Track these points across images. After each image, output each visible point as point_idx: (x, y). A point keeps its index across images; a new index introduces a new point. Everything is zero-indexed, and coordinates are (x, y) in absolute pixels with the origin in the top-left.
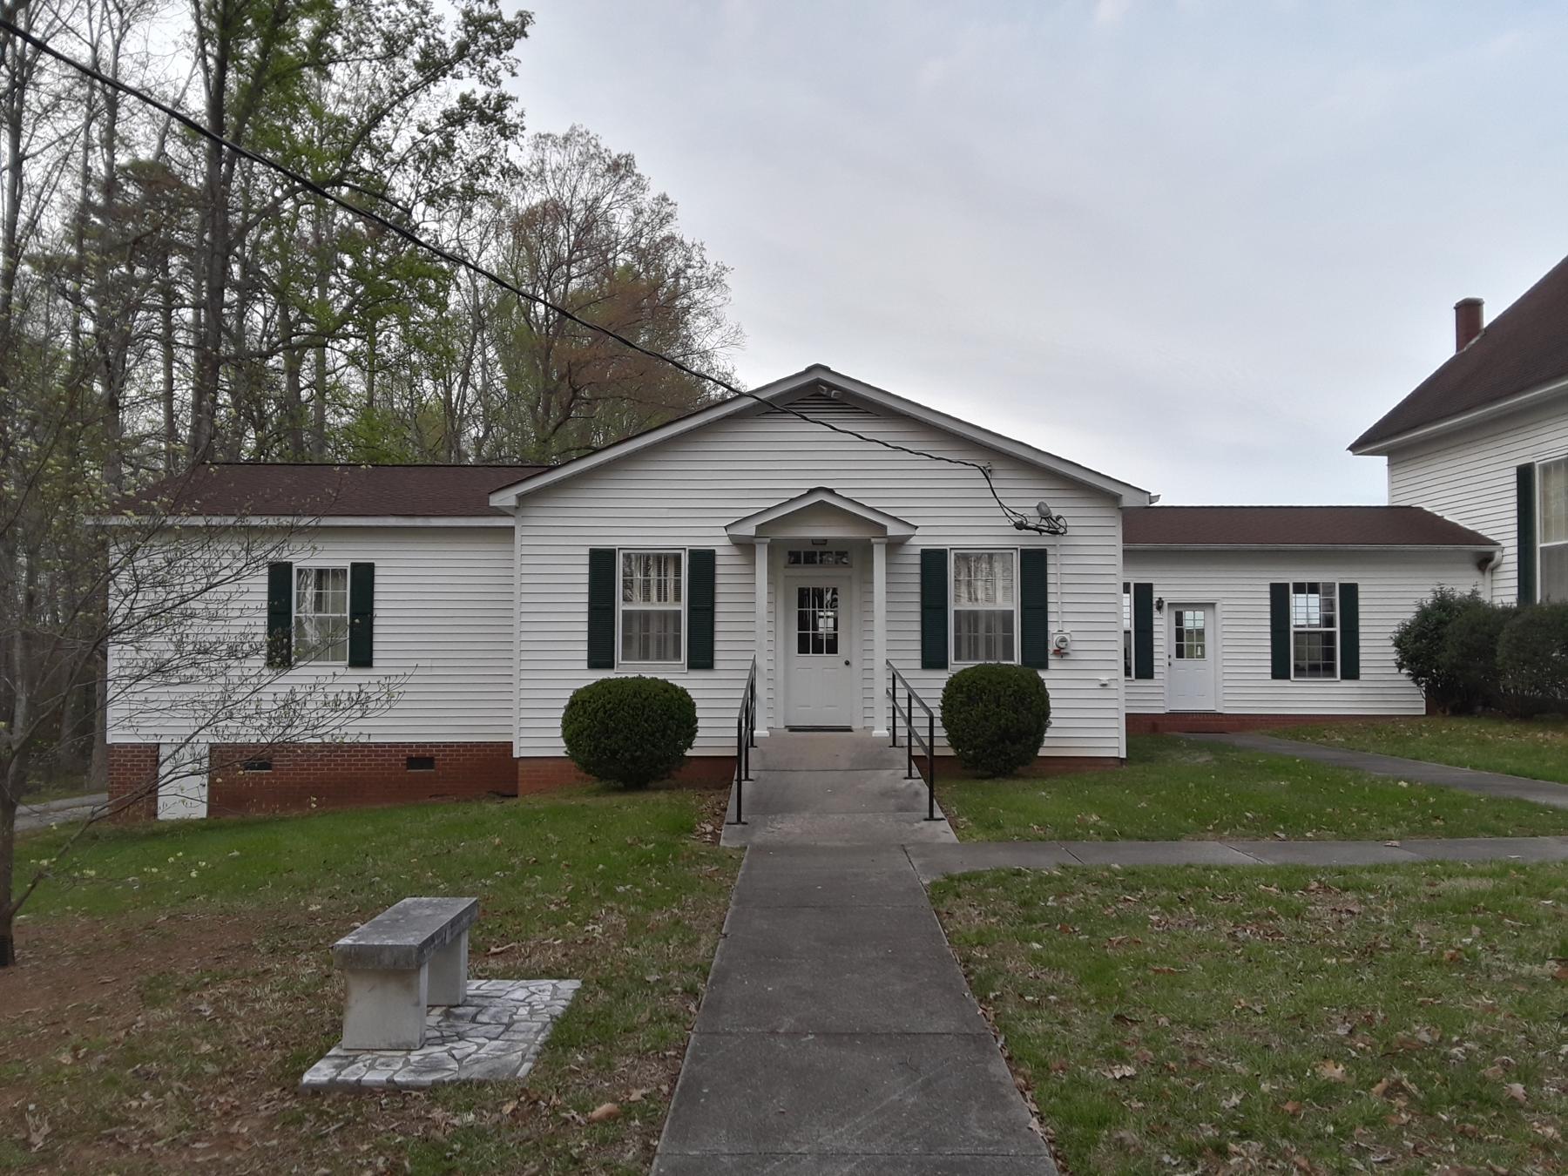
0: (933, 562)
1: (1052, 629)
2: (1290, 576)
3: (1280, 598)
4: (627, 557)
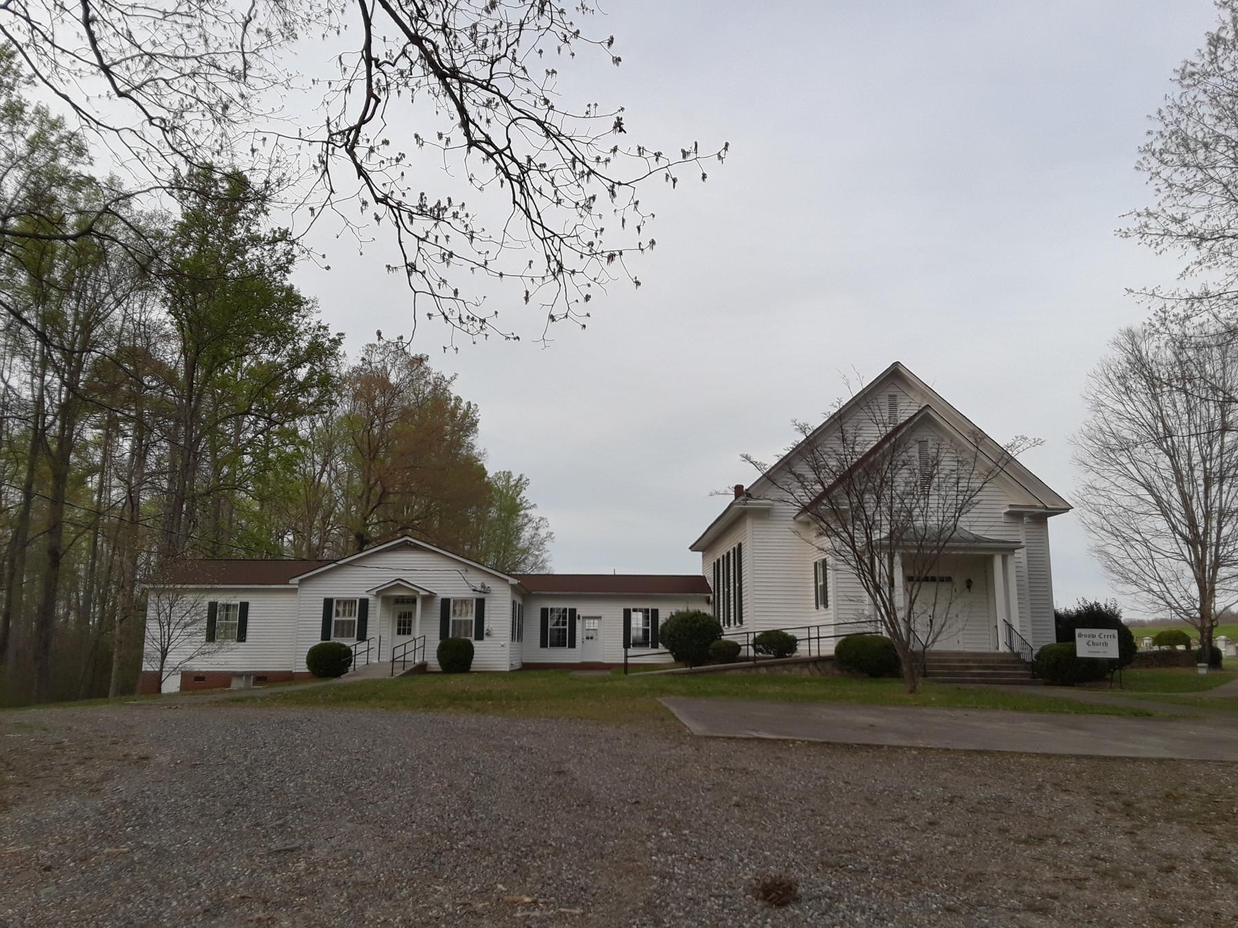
0: (445, 603)
1: (486, 626)
2: (631, 606)
3: (627, 615)
4: (338, 602)
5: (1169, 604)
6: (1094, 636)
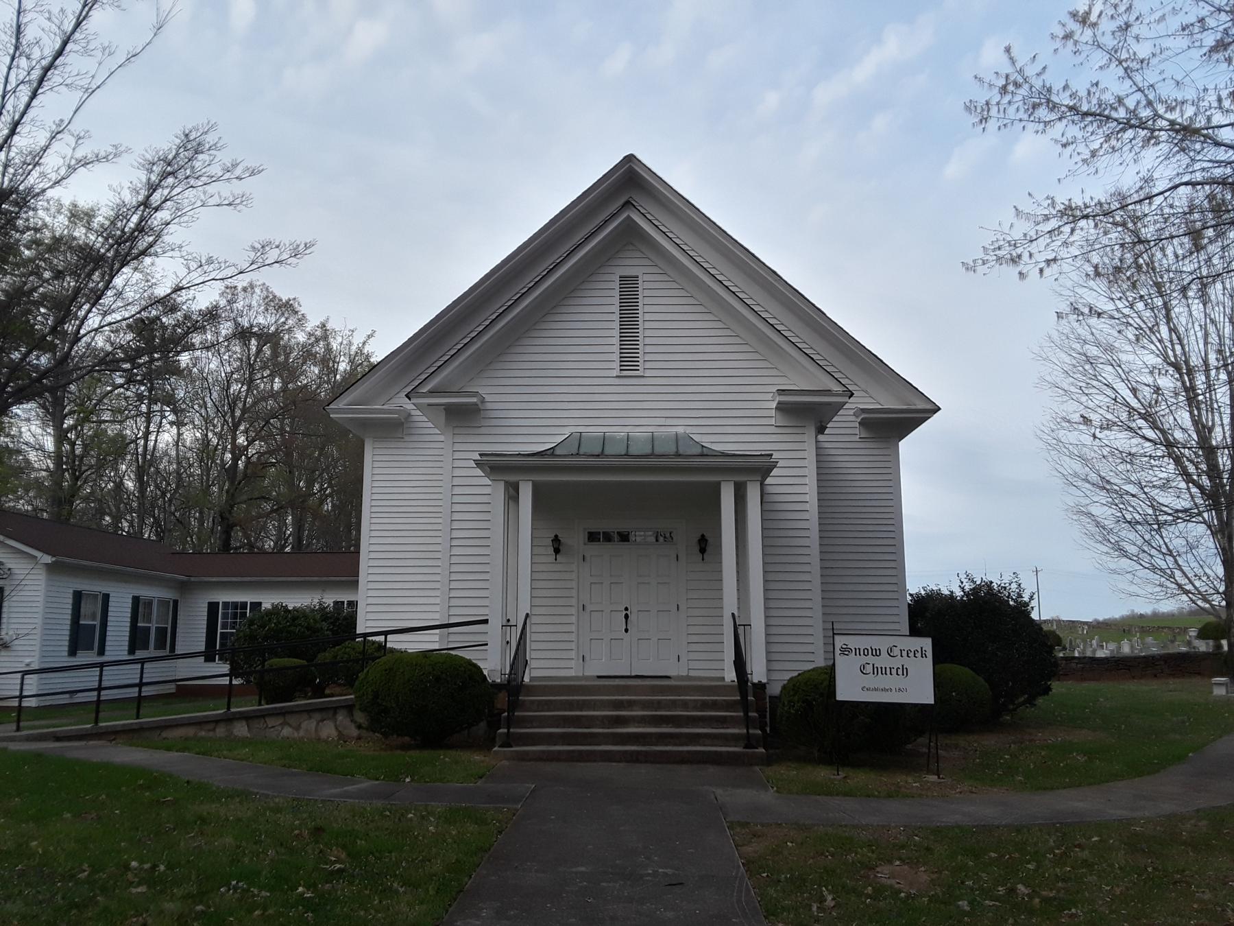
5: (1180, 586)
6: (876, 653)
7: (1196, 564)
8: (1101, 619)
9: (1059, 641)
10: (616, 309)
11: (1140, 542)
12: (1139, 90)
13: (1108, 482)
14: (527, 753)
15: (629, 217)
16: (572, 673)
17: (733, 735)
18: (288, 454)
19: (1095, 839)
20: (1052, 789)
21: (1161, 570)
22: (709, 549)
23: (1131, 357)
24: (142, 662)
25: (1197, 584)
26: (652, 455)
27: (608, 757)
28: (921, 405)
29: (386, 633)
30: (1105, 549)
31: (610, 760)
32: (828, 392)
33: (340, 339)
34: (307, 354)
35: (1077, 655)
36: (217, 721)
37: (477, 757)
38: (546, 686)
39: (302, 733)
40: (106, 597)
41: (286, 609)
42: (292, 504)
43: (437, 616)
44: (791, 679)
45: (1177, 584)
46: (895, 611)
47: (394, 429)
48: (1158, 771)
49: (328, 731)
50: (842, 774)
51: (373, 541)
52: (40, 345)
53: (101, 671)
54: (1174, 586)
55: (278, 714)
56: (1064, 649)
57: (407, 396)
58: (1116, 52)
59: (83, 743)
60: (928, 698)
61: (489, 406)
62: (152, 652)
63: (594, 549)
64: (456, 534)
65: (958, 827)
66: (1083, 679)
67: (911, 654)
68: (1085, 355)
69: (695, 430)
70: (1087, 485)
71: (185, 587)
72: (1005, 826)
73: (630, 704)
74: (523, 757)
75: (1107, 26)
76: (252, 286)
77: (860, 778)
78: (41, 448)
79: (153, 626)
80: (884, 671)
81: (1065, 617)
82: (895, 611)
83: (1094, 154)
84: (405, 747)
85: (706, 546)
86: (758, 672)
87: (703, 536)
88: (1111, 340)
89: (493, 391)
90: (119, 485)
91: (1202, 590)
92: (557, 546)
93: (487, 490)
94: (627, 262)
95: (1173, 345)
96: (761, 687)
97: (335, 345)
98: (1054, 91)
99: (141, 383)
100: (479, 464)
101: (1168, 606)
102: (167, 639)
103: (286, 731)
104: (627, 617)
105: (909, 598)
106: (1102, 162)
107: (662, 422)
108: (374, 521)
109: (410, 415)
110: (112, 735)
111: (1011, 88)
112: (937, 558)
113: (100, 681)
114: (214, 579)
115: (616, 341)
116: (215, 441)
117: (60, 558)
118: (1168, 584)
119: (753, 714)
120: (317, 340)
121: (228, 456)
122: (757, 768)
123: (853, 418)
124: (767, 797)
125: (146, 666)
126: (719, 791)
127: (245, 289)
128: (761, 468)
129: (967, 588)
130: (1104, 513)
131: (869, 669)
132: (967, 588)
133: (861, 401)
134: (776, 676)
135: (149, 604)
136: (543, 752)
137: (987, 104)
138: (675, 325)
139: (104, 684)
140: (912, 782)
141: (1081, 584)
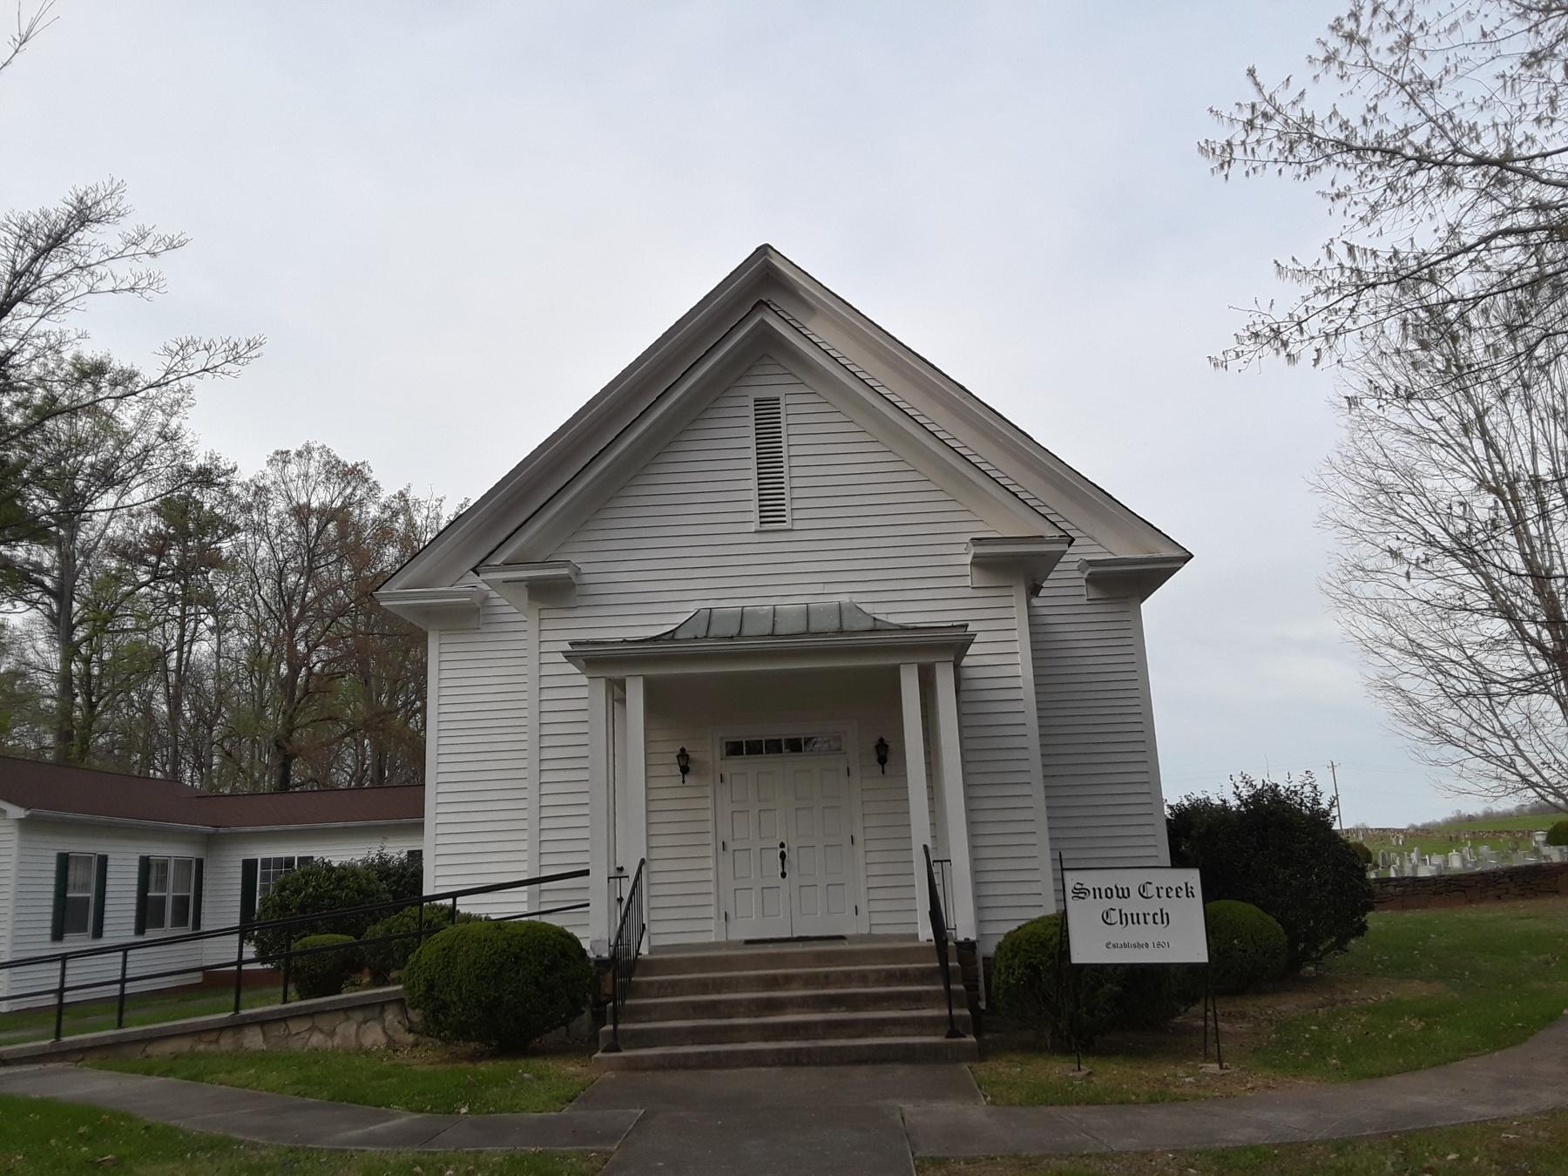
5: (1524, 779)
6: (1124, 894)
7: (1542, 748)
8: (1418, 824)
9: (1368, 856)
10: (752, 442)
11: (1465, 721)
12: (1430, 119)
13: (1419, 645)
14: (641, 1058)
15: (763, 321)
16: (712, 938)
17: (931, 1019)
18: (364, 663)
19: (1452, 1156)
20: (1381, 1076)
21: (1497, 757)
22: (891, 758)
23: (1438, 483)
24: (64, 958)
25: (1546, 773)
26: (807, 633)
27: (755, 1059)
28: (1167, 552)
29: (454, 895)
30: (1422, 734)
31: (759, 1064)
32: (1039, 539)
33: (425, 512)
34: (384, 532)
35: (1393, 875)
36: (221, 1029)
37: (572, 1068)
38: (671, 960)
39: (337, 1041)
40: (103, 860)
41: (329, 868)
42: (366, 726)
43: (525, 866)
44: (1009, 934)
45: (1520, 775)
46: (1148, 831)
47: (466, 618)
48: (1525, 1040)
49: (374, 1036)
50: (1085, 1069)
51: (443, 768)
52: (35, 532)
53: (125, 956)
54: (1515, 778)
55: (306, 1015)
56: (1376, 866)
57: (474, 570)
58: (1396, 72)
59: (37, 1067)
60: (1202, 956)
61: (587, 579)
62: (168, 931)
63: (735, 765)
64: (547, 754)
65: (1253, 1148)
66: (1404, 907)
67: (1172, 894)
68: (1378, 483)
69: (864, 598)
70: (1392, 652)
71: (211, 842)
72: (1324, 1142)
73: (787, 981)
74: (635, 1065)
75: (1382, 41)
76: (309, 450)
77: (1111, 1073)
78: (48, 670)
79: (170, 895)
80: (1135, 919)
81: (1373, 824)
82: (1148, 831)
83: (1374, 208)
84: (474, 1057)
85: (885, 753)
86: (963, 926)
87: (881, 740)
88: (1410, 462)
89: (585, 558)
90: (148, 711)
91: (1554, 781)
92: (685, 764)
93: (584, 693)
94: (762, 381)
95: (1491, 464)
96: (968, 947)
97: (419, 520)
98: (1318, 120)
99: (172, 579)
100: (570, 657)
101: (1508, 804)
102: (188, 911)
103: (316, 1039)
104: (783, 856)
105: (1167, 811)
106: (1386, 216)
107: (818, 589)
108: (442, 741)
109: (487, 598)
110: (80, 1053)
111: (1259, 122)
112: (1200, 763)
113: (124, 969)
114: (248, 829)
115: (753, 484)
116: (268, 649)
117: (36, 811)
118: (1507, 775)
119: (958, 987)
120: (395, 514)
121: (284, 669)
122: (965, 1066)
123: (1077, 574)
124: (975, 1112)
125: (69, 964)
126: (908, 1107)
127: (299, 454)
128: (954, 644)
129: (1245, 794)
130: (1423, 688)
131: (1115, 917)
132: (1245, 794)
133: (1086, 550)
134: (990, 929)
135: (163, 865)
136: (664, 1056)
137: (1229, 144)
138: (873, 489)
139: (130, 974)
140: (1181, 1075)
141: (1393, 784)
